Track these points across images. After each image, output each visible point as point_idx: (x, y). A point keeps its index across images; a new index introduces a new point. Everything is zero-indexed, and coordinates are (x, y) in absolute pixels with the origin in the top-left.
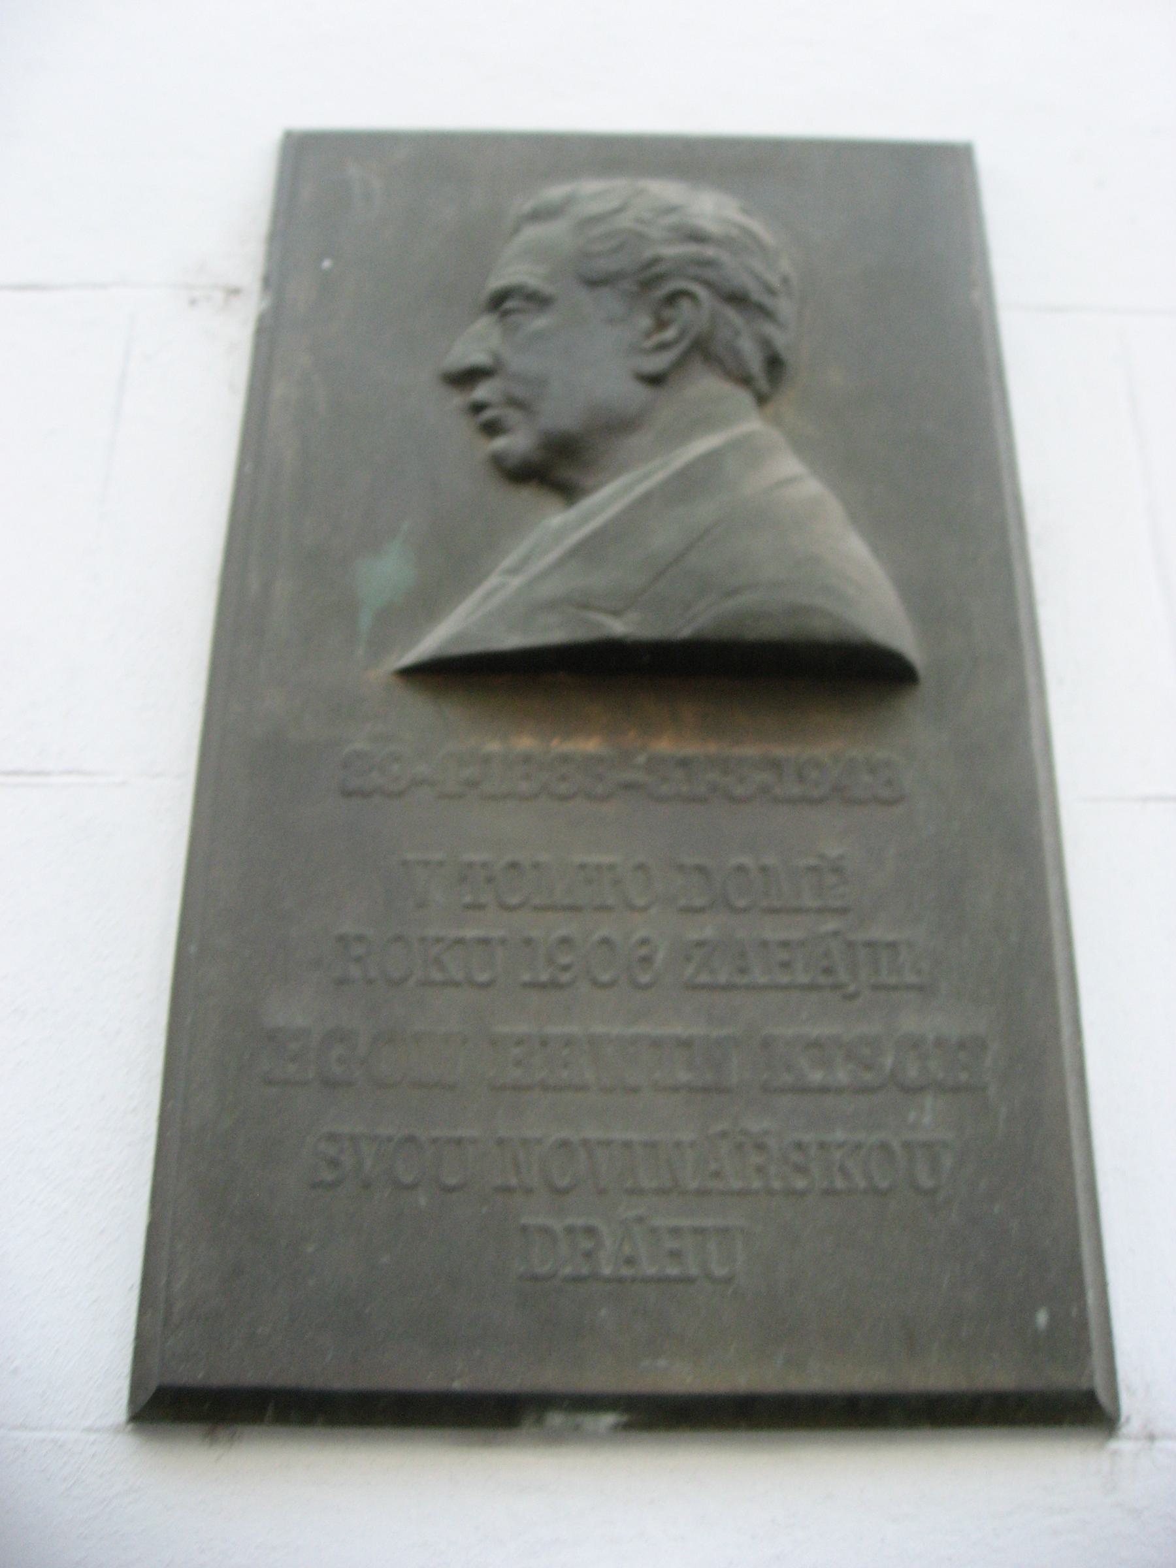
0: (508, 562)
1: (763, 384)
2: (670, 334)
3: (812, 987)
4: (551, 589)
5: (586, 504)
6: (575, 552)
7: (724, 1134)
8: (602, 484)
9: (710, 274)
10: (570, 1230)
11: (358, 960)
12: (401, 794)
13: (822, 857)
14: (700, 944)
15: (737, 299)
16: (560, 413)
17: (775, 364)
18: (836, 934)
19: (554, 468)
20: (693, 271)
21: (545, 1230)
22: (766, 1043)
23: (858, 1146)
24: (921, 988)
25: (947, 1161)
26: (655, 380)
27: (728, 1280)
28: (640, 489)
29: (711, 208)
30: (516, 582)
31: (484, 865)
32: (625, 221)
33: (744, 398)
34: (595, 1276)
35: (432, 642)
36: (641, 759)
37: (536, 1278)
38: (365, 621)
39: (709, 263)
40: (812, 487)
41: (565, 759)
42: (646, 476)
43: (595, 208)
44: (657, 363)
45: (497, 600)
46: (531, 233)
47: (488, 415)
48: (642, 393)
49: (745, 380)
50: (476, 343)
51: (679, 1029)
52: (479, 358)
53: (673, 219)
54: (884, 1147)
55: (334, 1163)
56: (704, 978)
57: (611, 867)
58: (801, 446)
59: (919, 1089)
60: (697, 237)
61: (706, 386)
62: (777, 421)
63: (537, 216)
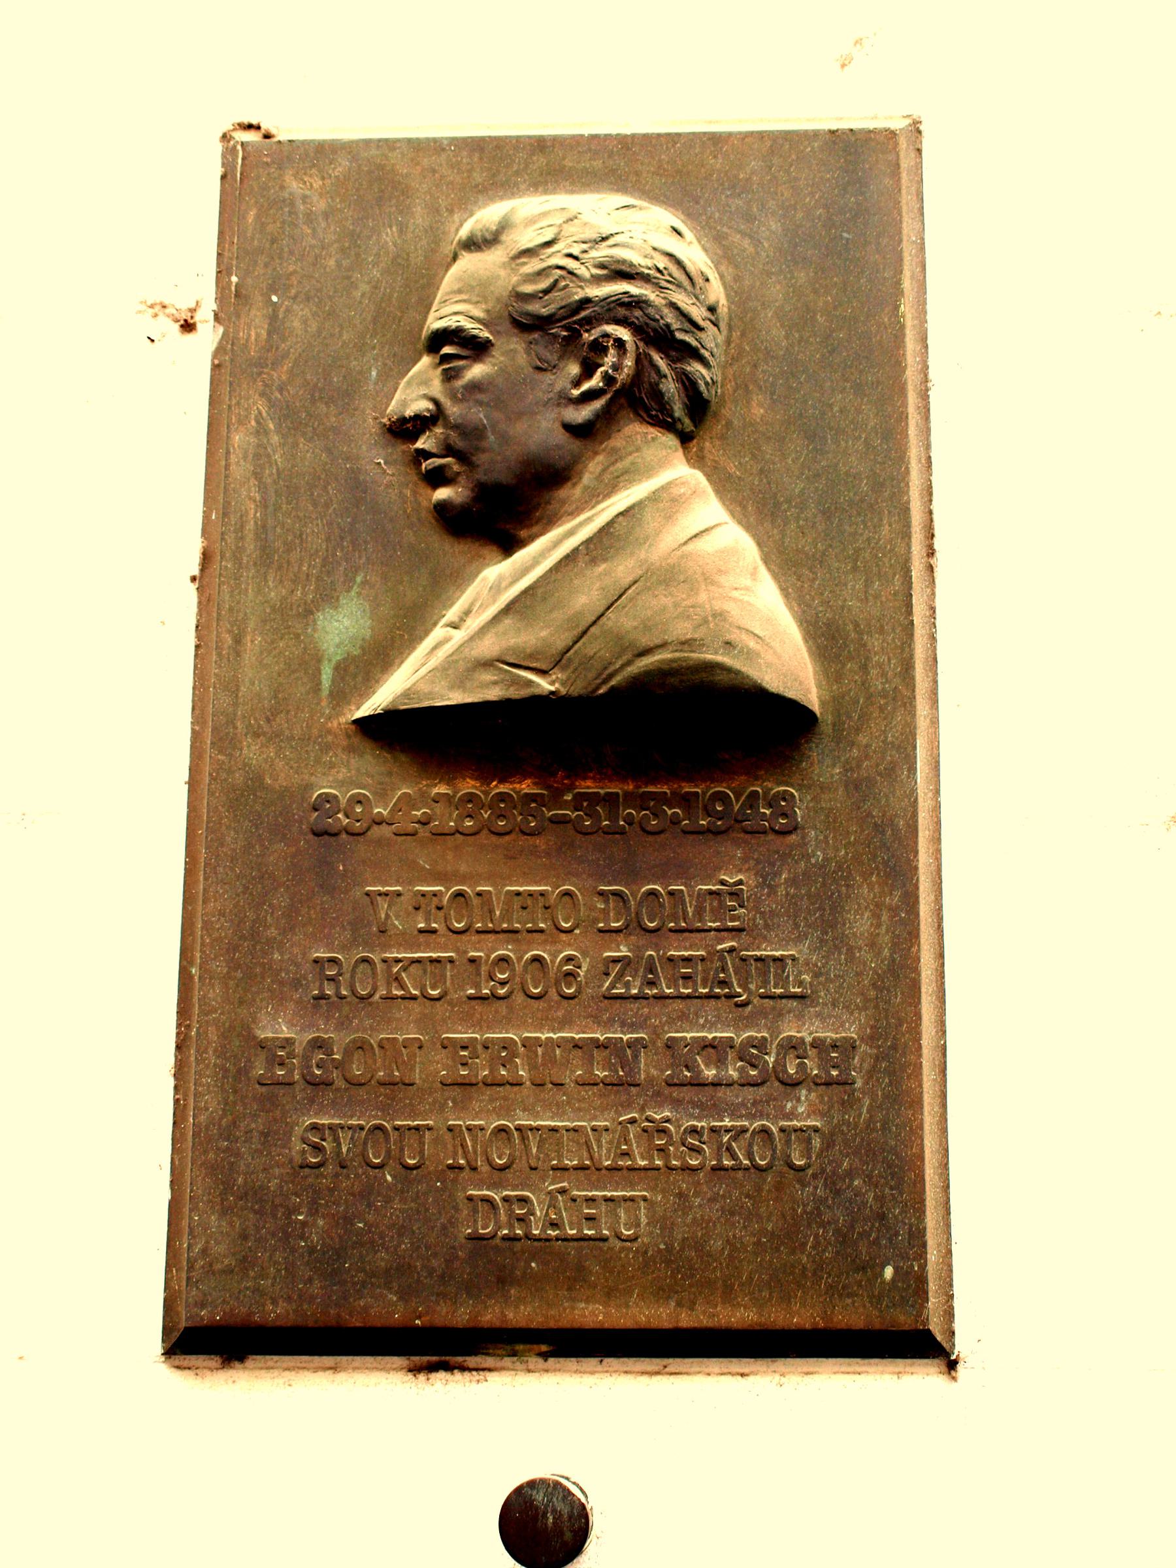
0: (452, 614)
2: (595, 382)
3: (708, 997)
4: (489, 647)
5: (521, 556)
6: (508, 610)
7: (633, 1121)
10: (506, 1199)
11: (331, 979)
12: (364, 833)
13: (723, 883)
14: (616, 960)
16: (497, 461)
17: (699, 406)
20: (622, 312)
21: (487, 1200)
22: (670, 1045)
23: (744, 1130)
24: (801, 997)
25: (817, 1142)
27: (633, 1239)
29: (645, 230)
30: (459, 636)
33: (671, 440)
34: (528, 1236)
36: (568, 797)
37: (482, 1238)
38: (327, 675)
39: (638, 303)
41: (502, 797)
42: (571, 533)
43: (528, 238)
45: (442, 654)
46: (468, 262)
47: (427, 465)
48: (574, 445)
49: (667, 423)
50: (417, 389)
53: (601, 253)
54: (765, 1131)
55: (317, 1148)
57: (542, 894)
59: (796, 1084)
60: (621, 272)
62: (697, 461)
63: (473, 244)
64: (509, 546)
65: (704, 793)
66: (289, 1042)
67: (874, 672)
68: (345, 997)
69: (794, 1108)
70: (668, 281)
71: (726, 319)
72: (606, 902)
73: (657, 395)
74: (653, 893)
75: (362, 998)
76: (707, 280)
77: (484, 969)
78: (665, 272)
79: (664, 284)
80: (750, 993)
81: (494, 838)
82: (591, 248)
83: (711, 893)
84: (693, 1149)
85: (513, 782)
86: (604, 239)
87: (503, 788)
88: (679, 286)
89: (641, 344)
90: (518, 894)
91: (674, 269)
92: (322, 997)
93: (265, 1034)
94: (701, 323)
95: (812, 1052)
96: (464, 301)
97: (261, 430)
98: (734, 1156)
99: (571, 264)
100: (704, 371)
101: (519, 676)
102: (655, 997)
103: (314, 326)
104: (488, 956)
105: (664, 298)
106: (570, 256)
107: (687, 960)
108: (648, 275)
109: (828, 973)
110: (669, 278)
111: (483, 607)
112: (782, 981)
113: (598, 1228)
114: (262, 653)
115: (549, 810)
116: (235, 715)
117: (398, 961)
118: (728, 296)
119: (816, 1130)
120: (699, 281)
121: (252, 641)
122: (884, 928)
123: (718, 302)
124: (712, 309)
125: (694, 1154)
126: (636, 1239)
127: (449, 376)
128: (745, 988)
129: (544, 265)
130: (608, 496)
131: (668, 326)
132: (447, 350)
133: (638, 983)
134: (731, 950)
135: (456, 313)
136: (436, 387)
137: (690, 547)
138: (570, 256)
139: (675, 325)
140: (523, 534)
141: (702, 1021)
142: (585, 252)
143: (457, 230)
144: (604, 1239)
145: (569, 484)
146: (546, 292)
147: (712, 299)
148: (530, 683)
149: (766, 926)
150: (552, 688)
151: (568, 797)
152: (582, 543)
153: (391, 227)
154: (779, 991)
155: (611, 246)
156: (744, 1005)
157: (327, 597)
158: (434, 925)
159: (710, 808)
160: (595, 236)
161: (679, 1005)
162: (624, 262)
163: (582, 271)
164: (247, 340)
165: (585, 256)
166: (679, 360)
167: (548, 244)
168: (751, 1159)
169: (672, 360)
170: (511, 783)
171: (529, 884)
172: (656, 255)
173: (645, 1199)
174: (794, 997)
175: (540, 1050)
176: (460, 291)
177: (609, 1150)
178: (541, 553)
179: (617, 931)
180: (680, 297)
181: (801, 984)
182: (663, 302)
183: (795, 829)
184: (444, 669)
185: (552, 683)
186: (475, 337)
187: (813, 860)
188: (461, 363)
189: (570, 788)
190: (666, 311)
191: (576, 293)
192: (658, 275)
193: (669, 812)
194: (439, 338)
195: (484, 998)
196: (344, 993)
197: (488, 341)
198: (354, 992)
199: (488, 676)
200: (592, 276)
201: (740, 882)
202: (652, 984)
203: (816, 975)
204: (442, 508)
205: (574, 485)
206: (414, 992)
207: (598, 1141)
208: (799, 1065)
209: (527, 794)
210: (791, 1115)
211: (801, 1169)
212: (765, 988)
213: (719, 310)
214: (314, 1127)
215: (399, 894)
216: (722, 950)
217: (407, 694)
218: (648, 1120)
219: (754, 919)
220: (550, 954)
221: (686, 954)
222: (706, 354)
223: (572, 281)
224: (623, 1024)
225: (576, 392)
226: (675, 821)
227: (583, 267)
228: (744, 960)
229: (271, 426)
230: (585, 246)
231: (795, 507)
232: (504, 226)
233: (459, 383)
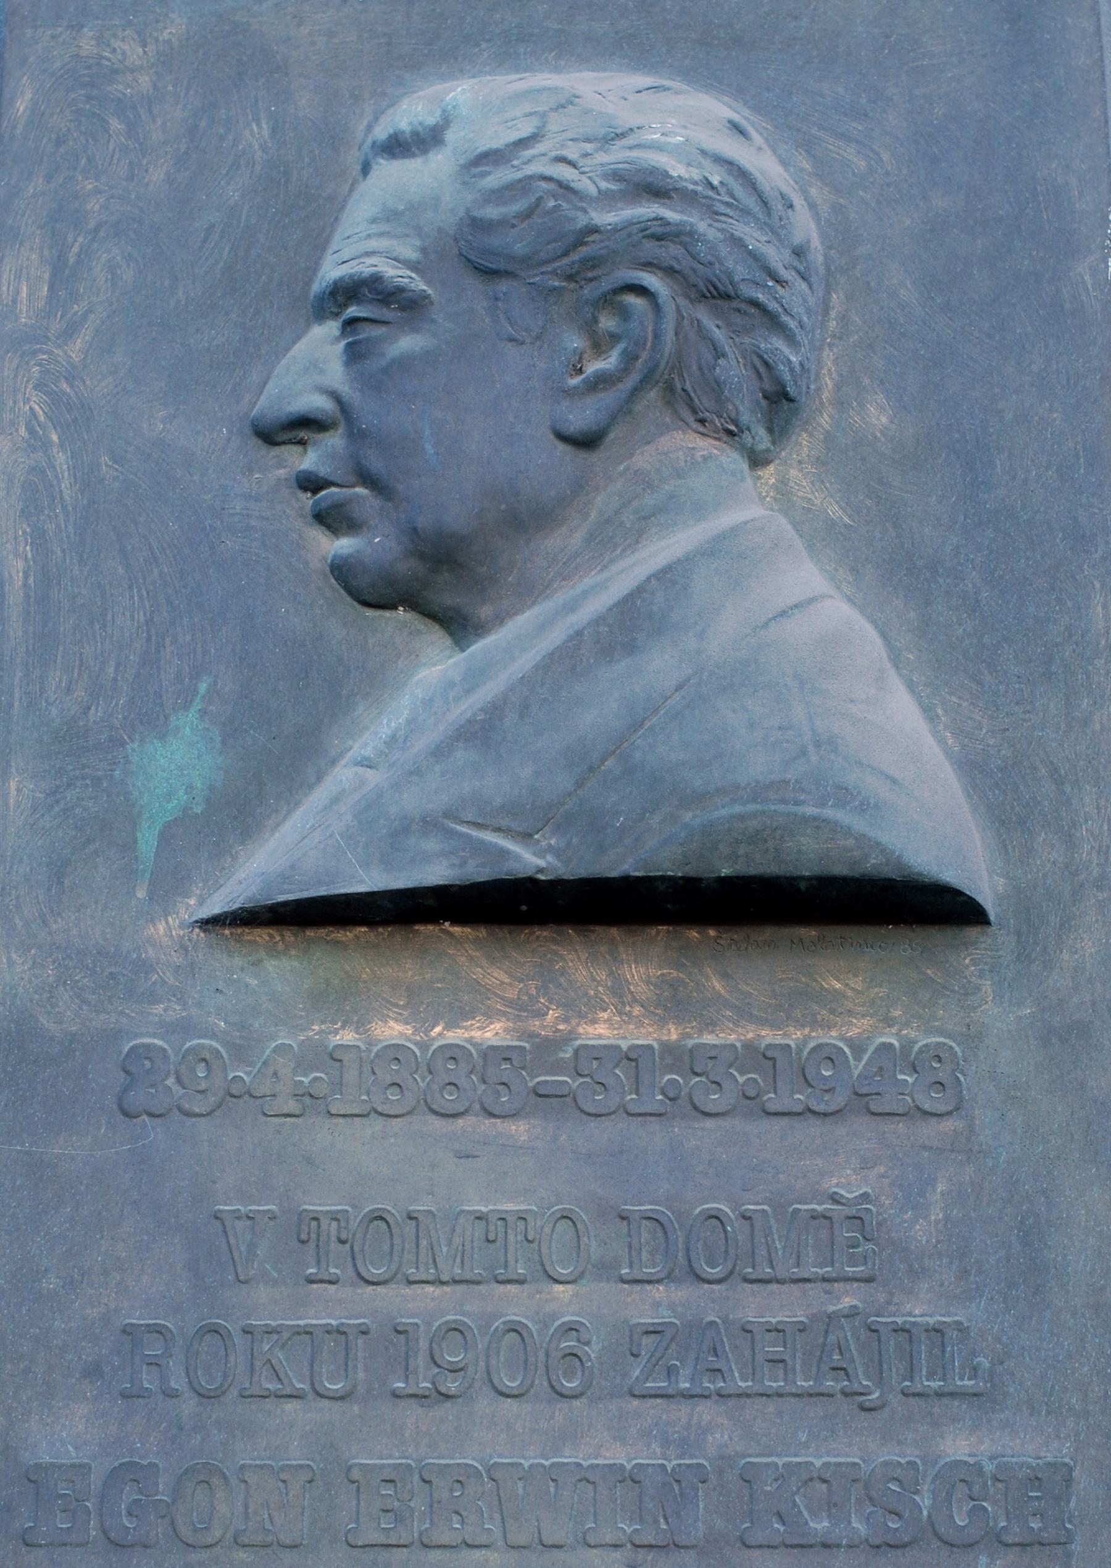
8: (500, 619)
9: (671, 252)
11: (154, 1363)
13: (835, 1199)
15: (717, 294)
18: (852, 1314)
19: (436, 583)
20: (650, 249)
26: (586, 442)
28: (556, 636)
31: (334, 1217)
32: (536, 163)
33: (732, 459)
38: (147, 841)
40: (839, 612)
42: (571, 607)
44: (581, 416)
46: (391, 175)
50: (311, 366)
51: (618, 1455)
53: (616, 155)
58: (820, 536)
60: (654, 187)
63: (397, 147)
71: (822, 270)
78: (722, 190)
79: (722, 209)
81: (437, 1123)
82: (597, 150)
83: (814, 1216)
87: (455, 1036)
88: (746, 212)
89: (681, 301)
94: (784, 274)
96: (382, 234)
97: (36, 441)
99: (564, 172)
100: (786, 351)
101: (482, 842)
103: (128, 275)
104: (429, 1324)
105: (722, 230)
108: (695, 193)
112: (939, 1369)
114: (34, 809)
115: (532, 1077)
118: (824, 236)
120: (778, 206)
123: (808, 242)
124: (799, 252)
127: (354, 354)
128: (880, 1382)
131: (730, 275)
132: (353, 311)
135: (368, 254)
136: (336, 374)
139: (740, 272)
140: (485, 612)
143: (369, 128)
145: (564, 529)
147: (798, 239)
148: (503, 853)
150: (542, 863)
153: (257, 121)
154: (935, 1384)
155: (630, 148)
157: (151, 720)
158: (333, 1270)
159: (810, 1074)
160: (602, 132)
162: (653, 171)
164: (14, 301)
165: (588, 161)
166: (748, 330)
167: (522, 143)
172: (707, 163)
178: (519, 640)
180: (747, 229)
181: (975, 1371)
185: (540, 854)
186: (401, 290)
188: (381, 330)
192: (711, 193)
193: (741, 1079)
194: (347, 292)
197: (425, 297)
204: (342, 571)
206: (299, 1386)
212: (911, 1379)
213: (811, 257)
220: (684, 1080)
222: (793, 324)
223: (569, 202)
227: (583, 178)
229: (55, 438)
230: (589, 147)
233: (374, 365)
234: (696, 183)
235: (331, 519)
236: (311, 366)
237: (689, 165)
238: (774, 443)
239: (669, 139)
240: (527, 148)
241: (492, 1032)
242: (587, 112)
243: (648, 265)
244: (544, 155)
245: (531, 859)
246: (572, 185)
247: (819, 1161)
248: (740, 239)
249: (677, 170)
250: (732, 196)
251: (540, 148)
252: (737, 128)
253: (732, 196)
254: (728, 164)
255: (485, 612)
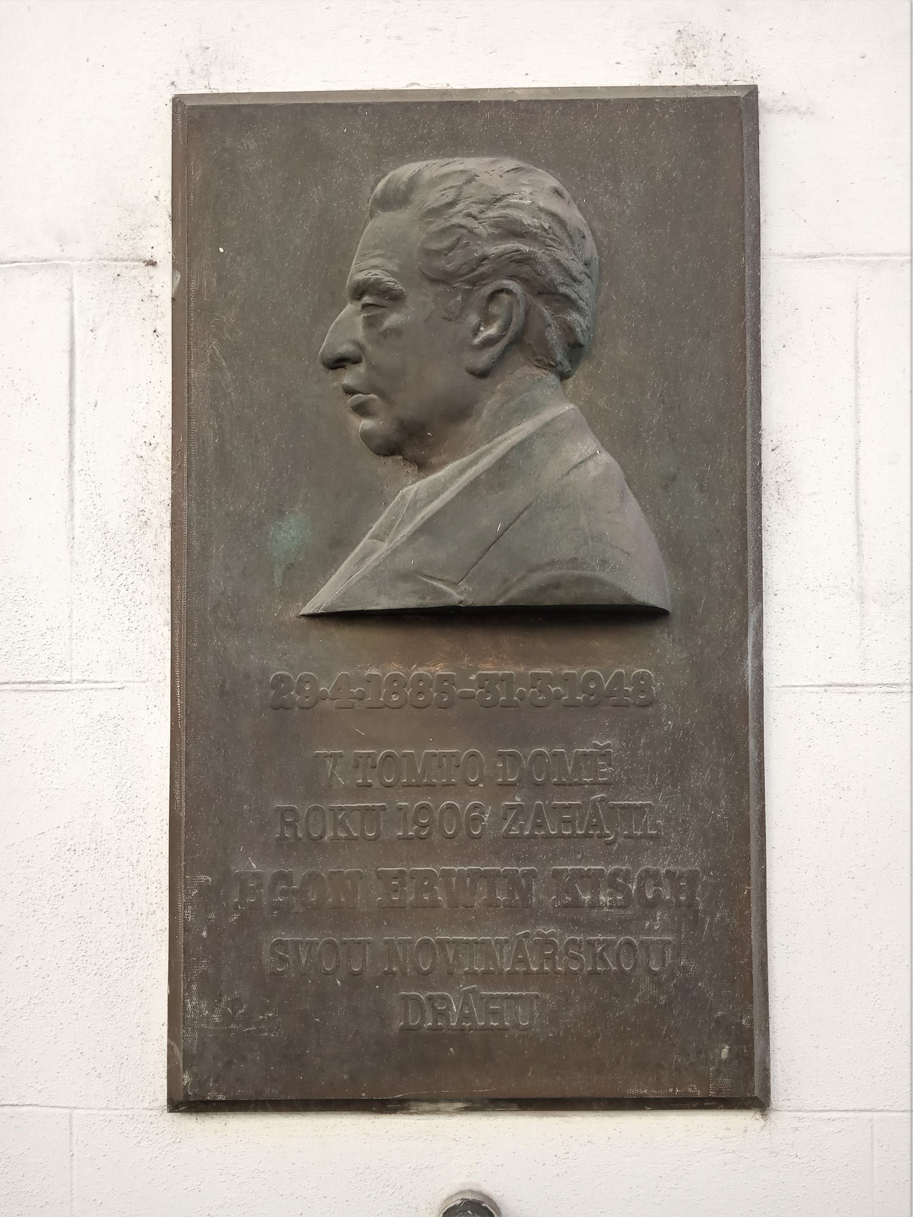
1: (567, 366)
4: (408, 560)
6: (426, 528)
7: (526, 936)
10: (430, 998)
13: (595, 746)
14: (511, 808)
16: (411, 402)
17: (576, 350)
19: (411, 443)
20: (513, 268)
21: (416, 998)
23: (613, 943)
25: (669, 953)
26: (482, 374)
28: (471, 473)
29: (531, 191)
30: (384, 547)
33: (552, 379)
35: (325, 597)
39: (526, 260)
41: (420, 678)
43: (434, 198)
45: (371, 562)
46: (384, 220)
49: (552, 367)
50: (347, 326)
52: (345, 348)
54: (629, 943)
56: (515, 832)
61: (523, 374)
64: (423, 466)
65: (580, 674)
66: (256, 875)
67: (714, 574)
68: (300, 839)
69: (651, 926)
70: (551, 239)
72: (504, 762)
73: (543, 343)
74: (541, 754)
75: (314, 840)
76: (584, 237)
77: (410, 815)
79: (550, 242)
80: (617, 833)
84: (575, 958)
85: (428, 666)
86: (498, 200)
87: (421, 671)
89: (529, 296)
90: (435, 755)
91: (557, 228)
92: (283, 838)
93: (237, 869)
94: (579, 277)
95: (666, 882)
98: (606, 964)
102: (543, 837)
105: (549, 255)
106: (469, 215)
107: (568, 807)
109: (677, 819)
110: (552, 236)
111: (403, 523)
113: (501, 1020)
116: (206, 610)
117: (342, 809)
119: (669, 942)
120: (577, 239)
121: (217, 548)
122: (721, 783)
125: (575, 961)
126: (531, 1028)
127: (370, 323)
129: (448, 224)
130: (502, 432)
131: (552, 280)
133: (529, 826)
134: (602, 800)
136: (360, 333)
137: (572, 477)
138: (469, 215)
139: (559, 279)
140: (434, 460)
141: (579, 856)
142: (482, 212)
143: (373, 189)
144: (506, 1029)
146: (451, 248)
147: (587, 256)
148: (442, 593)
149: (629, 781)
150: (462, 598)
151: (473, 677)
152: (483, 472)
156: (611, 843)
160: (489, 197)
161: (561, 843)
163: (481, 230)
165: (483, 216)
167: (451, 204)
168: (619, 966)
169: (556, 311)
170: (428, 666)
171: (443, 748)
172: (542, 216)
173: (537, 997)
174: (651, 837)
175: (454, 880)
176: (376, 247)
177: (508, 959)
178: (450, 477)
179: (513, 784)
181: (655, 826)
182: (548, 259)
183: (652, 703)
184: (373, 576)
185: (461, 593)
186: (390, 289)
187: (666, 728)
188: (383, 310)
189: (475, 670)
190: (551, 267)
191: (476, 251)
193: (553, 690)
194: (359, 291)
195: (410, 838)
196: (300, 835)
198: (308, 835)
199: (407, 586)
200: (489, 234)
201: (608, 746)
202: (539, 826)
203: (668, 820)
204: (366, 436)
205: (476, 420)
207: (501, 951)
208: (655, 891)
209: (440, 676)
210: (650, 931)
211: (656, 974)
214: (280, 943)
215: (341, 755)
216: (594, 801)
217: (344, 595)
218: (538, 934)
219: (620, 775)
221: (567, 803)
224: (518, 859)
225: (477, 341)
226: (558, 696)
228: (613, 808)
231: (652, 436)
232: (412, 184)
234: (537, 228)
235: (361, 410)
236: (347, 326)
237: (533, 217)
238: (572, 367)
239: (523, 202)
240: (451, 208)
241: (439, 670)
242: (482, 185)
243: (512, 277)
244: (460, 212)
245: (456, 596)
246: (475, 230)
247: (734, 621)
248: (558, 260)
249: (528, 220)
250: (554, 234)
251: (458, 207)
252: (557, 192)
253: (554, 234)
254: (553, 215)
255: (434, 460)
